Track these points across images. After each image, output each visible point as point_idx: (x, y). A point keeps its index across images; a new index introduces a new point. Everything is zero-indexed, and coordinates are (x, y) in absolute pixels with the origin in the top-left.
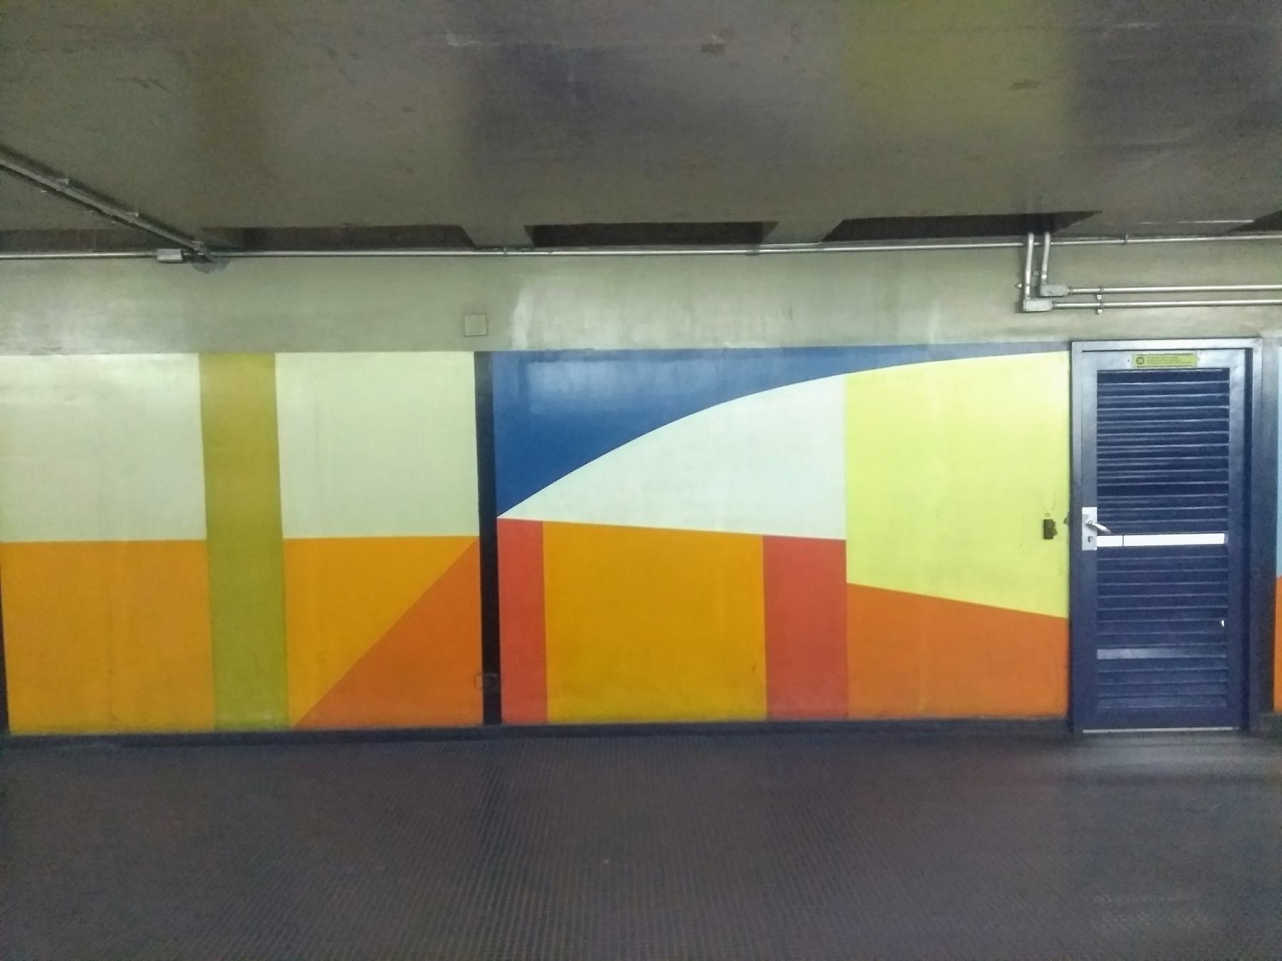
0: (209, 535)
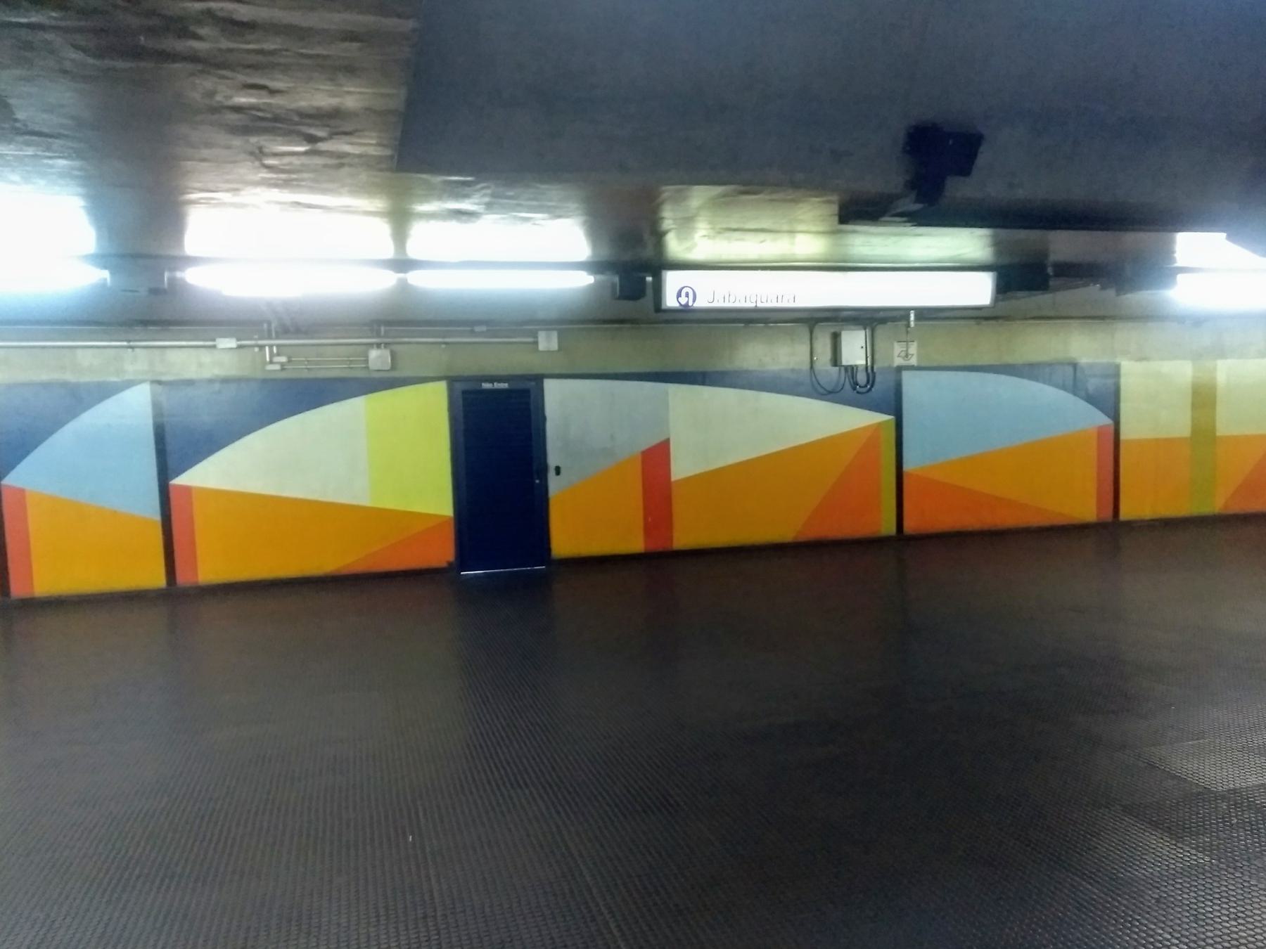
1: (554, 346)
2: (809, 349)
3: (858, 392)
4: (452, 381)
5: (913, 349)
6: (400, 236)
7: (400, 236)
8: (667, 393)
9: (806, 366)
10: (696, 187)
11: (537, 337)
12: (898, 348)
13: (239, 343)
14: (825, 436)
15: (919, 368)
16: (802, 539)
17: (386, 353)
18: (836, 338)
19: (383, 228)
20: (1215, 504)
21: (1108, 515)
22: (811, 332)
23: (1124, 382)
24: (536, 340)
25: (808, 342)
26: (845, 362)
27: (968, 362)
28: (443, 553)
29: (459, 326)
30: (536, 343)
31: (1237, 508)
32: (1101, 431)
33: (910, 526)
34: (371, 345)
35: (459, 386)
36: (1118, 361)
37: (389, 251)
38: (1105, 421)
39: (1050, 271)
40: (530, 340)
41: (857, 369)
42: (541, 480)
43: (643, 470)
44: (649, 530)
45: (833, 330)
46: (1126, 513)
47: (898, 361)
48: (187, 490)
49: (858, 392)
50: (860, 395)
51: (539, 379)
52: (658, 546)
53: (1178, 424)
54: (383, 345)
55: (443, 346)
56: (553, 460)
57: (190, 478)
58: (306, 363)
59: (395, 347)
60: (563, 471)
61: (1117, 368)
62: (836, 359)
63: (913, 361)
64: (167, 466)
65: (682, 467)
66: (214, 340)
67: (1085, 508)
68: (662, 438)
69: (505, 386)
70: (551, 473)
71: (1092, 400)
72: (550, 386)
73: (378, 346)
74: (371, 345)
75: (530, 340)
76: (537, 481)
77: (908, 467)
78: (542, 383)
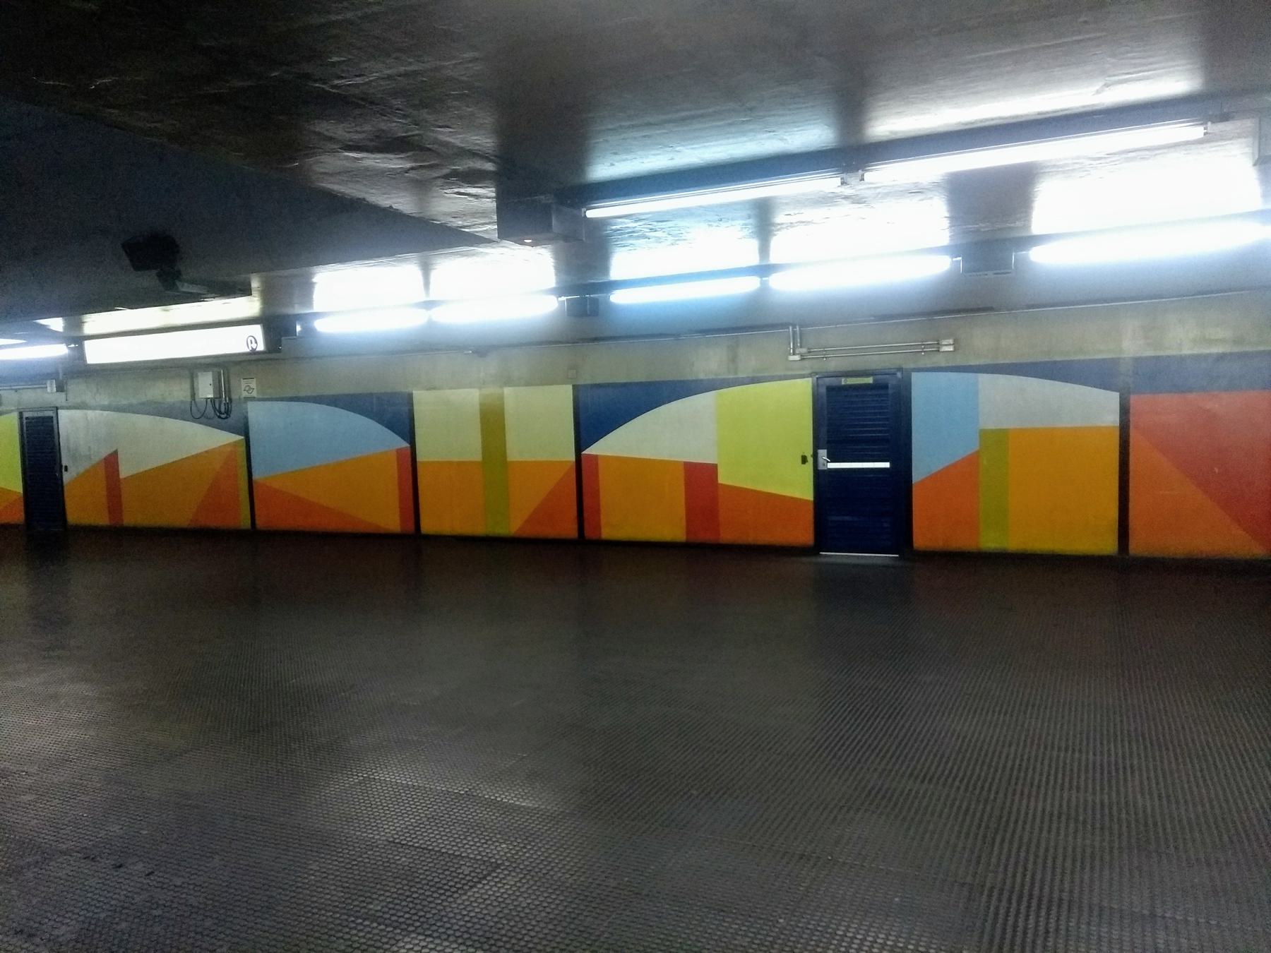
0: (483, 458)
5: (253, 384)
6: (764, 249)
7: (764, 249)
9: (189, 399)
12: (243, 383)
15: (259, 400)
16: (525, 535)
19: (754, 244)
20: (511, 525)
21: (411, 528)
23: (417, 409)
28: (18, 516)
29: (1096, 303)
31: (531, 532)
32: (399, 452)
33: (1137, 547)
36: (409, 390)
37: (751, 256)
38: (405, 445)
39: (764, 279)
46: (429, 525)
47: (245, 394)
48: (595, 458)
50: (220, 420)
53: (470, 448)
57: (591, 451)
60: (800, 460)
61: (410, 396)
63: (254, 394)
64: (579, 447)
65: (125, 471)
67: (390, 520)
69: (870, 380)
71: (392, 425)
77: (256, 476)
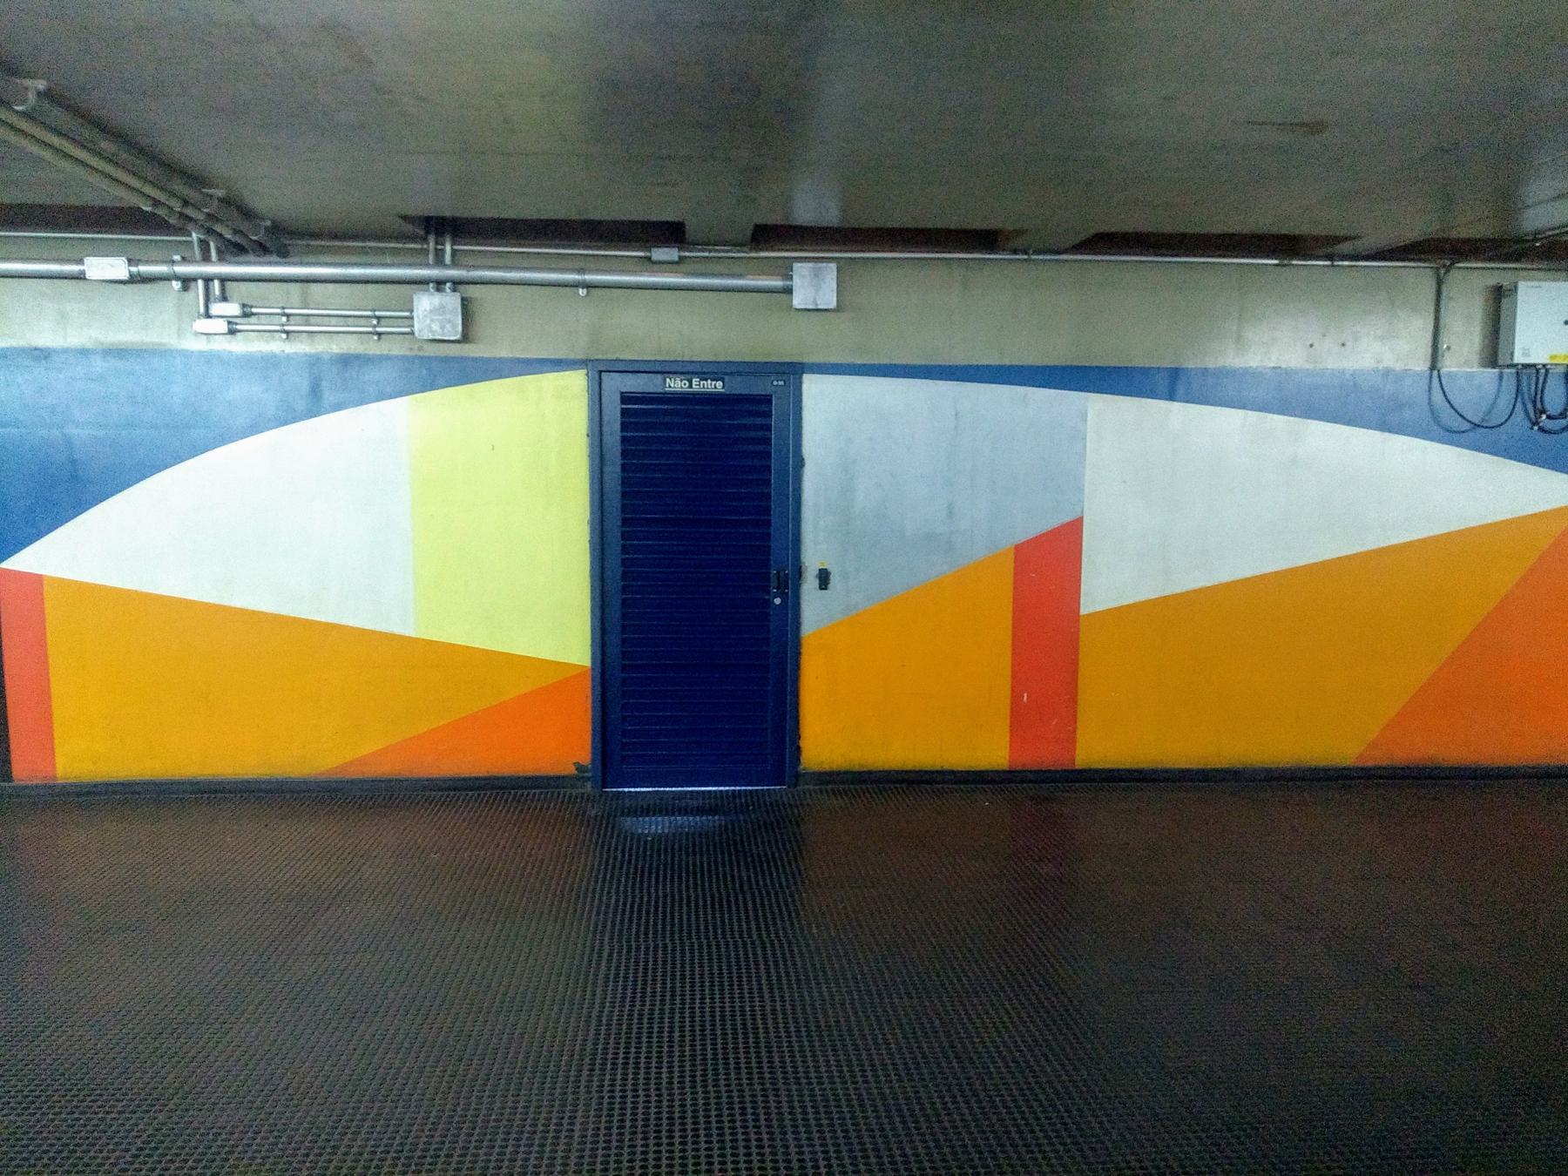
1: (829, 299)
2: (1431, 327)
3: (1542, 430)
4: (599, 370)
8: (1079, 437)
10: (1006, 768)
11: (791, 278)
13: (134, 269)
14: (1454, 527)
17: (452, 301)
18: (1499, 298)
22: (1439, 283)
24: (789, 283)
25: (1432, 309)
26: (1519, 358)
27: (993, 359)
30: (788, 291)
34: (422, 282)
35: (616, 385)
40: (777, 283)
41: (1547, 370)
42: (784, 597)
43: (1015, 601)
44: (1019, 719)
45: (1493, 279)
49: (1542, 430)
51: (793, 371)
52: (1044, 757)
54: (448, 285)
55: (582, 292)
56: (813, 557)
58: (375, 322)
59: (472, 291)
60: (835, 580)
62: (1494, 350)
66: (80, 262)
68: (1066, 518)
70: (809, 584)
72: (814, 388)
73: (439, 284)
74: (422, 282)
75: (777, 283)
76: (778, 601)
78: (801, 378)
